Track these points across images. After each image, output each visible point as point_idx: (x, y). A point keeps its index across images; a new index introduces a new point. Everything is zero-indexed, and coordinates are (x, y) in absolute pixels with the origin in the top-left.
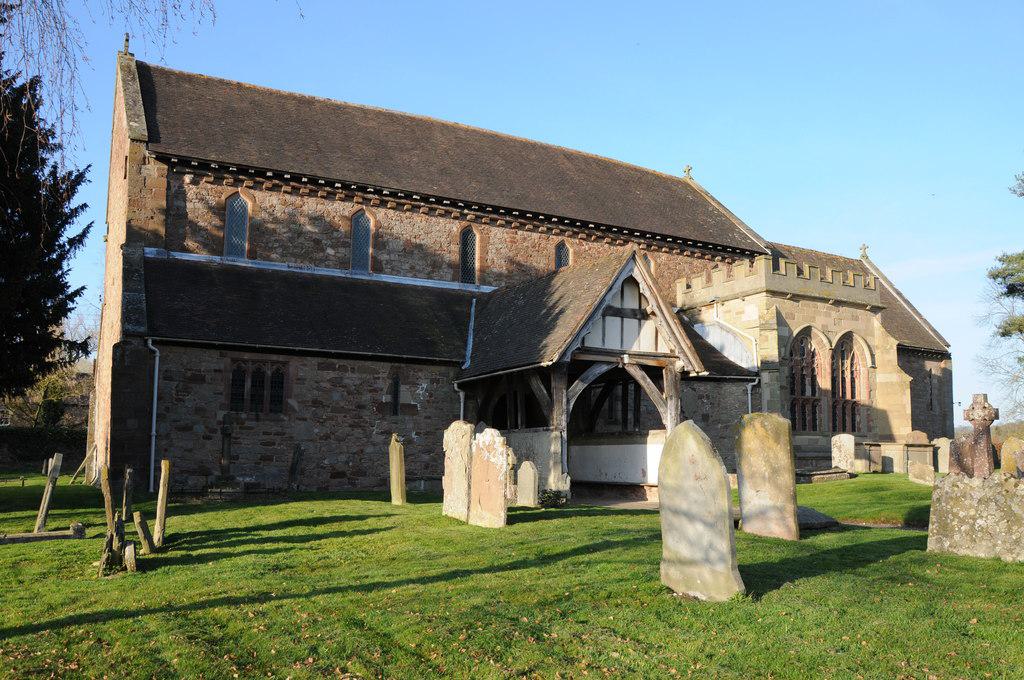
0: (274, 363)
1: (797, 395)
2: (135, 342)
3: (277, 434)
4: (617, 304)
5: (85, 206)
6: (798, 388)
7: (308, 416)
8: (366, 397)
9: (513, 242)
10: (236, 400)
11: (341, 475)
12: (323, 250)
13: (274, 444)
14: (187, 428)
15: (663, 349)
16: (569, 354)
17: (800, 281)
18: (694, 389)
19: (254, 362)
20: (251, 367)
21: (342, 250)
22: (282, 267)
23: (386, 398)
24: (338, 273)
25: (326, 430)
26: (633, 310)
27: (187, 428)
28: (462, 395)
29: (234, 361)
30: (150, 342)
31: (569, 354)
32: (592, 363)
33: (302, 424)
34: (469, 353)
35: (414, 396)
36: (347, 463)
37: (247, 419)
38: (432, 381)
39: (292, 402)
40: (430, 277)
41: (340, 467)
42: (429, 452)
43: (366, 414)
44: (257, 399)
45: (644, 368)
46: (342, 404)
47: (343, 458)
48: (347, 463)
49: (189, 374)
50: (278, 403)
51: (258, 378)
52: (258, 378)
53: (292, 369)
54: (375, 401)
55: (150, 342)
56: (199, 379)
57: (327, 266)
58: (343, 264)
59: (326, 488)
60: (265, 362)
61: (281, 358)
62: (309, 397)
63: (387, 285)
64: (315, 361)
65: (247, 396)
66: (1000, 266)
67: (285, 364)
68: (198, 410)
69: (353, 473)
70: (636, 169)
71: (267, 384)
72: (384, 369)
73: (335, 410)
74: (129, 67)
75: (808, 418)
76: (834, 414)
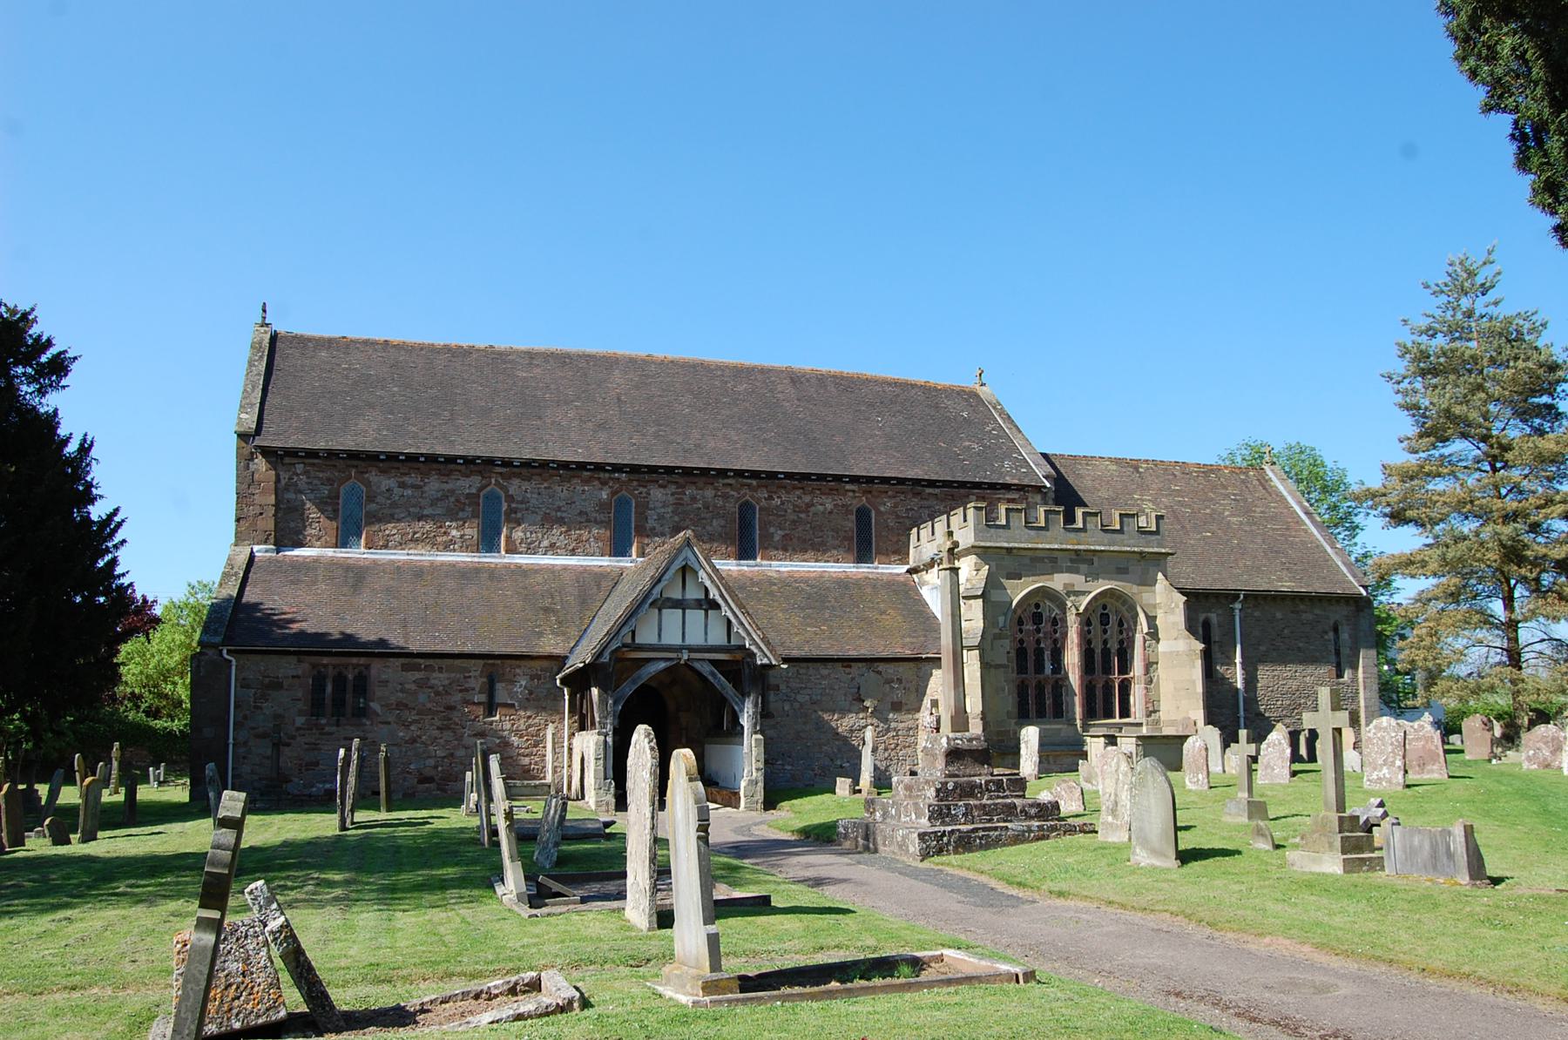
2: (210, 652)
5: (124, 541)
9: (678, 504)
11: (430, 780)
16: (607, 655)
18: (879, 673)
20: (331, 672)
26: (698, 601)
29: (314, 666)
31: (607, 655)
33: (385, 728)
35: (512, 695)
36: (436, 767)
37: (328, 724)
38: (532, 679)
39: (374, 705)
40: (573, 552)
41: (428, 772)
44: (339, 703)
45: (713, 662)
46: (429, 706)
47: (431, 762)
48: (436, 767)
51: (340, 680)
52: (340, 680)
53: (373, 672)
56: (277, 685)
58: (466, 548)
59: (413, 795)
61: (362, 660)
62: (393, 700)
63: (519, 567)
65: (328, 701)
69: (442, 779)
70: (896, 384)
71: (350, 688)
74: (260, 343)
75: (1048, 702)
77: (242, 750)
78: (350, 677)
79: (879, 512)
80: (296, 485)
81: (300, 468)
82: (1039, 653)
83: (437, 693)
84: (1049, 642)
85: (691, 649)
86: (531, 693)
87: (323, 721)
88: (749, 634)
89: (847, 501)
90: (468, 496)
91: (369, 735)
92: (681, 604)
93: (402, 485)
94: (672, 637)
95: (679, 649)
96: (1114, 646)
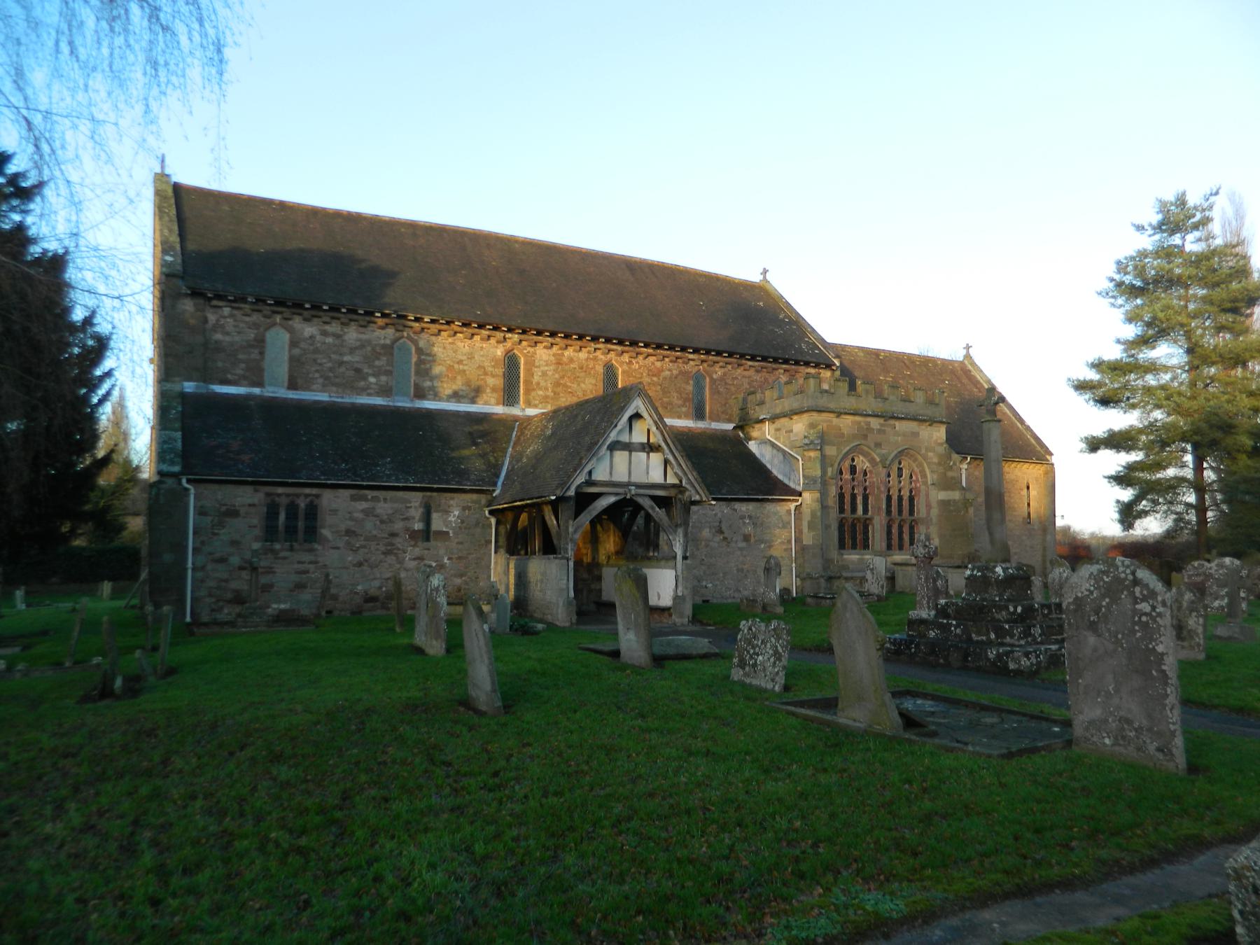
0: (307, 496)
1: (848, 514)
2: (170, 482)
3: (311, 563)
4: (625, 438)
6: (847, 506)
7: (341, 545)
8: (398, 526)
10: (270, 532)
12: (365, 379)
13: (308, 572)
14: (222, 560)
15: (671, 480)
17: (853, 399)
19: (288, 495)
20: (284, 501)
21: (384, 378)
22: (323, 397)
23: (418, 526)
24: (379, 401)
25: (360, 557)
26: (642, 444)
27: (222, 560)
28: (493, 521)
29: (268, 495)
30: (184, 481)
32: (598, 495)
34: (500, 483)
35: (447, 523)
36: (380, 588)
37: (282, 550)
38: (464, 509)
41: (373, 592)
42: (461, 576)
43: (398, 541)
45: (653, 498)
46: (374, 532)
47: (377, 583)
49: (224, 509)
50: (312, 533)
51: (292, 510)
52: (292, 510)
54: (407, 529)
55: (184, 481)
56: (233, 513)
57: (369, 395)
60: (298, 496)
61: (315, 491)
62: (343, 527)
64: (346, 493)
66: (1093, 376)
67: (317, 496)
68: (234, 543)
72: (416, 499)
73: (367, 539)
76: (889, 533)
77: (199, 574)
78: (302, 505)
79: (711, 378)
80: (223, 326)
81: (227, 311)
82: (854, 497)
83: (382, 522)
84: (861, 489)
85: (638, 486)
86: (462, 522)
87: (277, 546)
88: (685, 474)
89: (687, 367)
90: (384, 346)
91: (320, 559)
92: (629, 447)
93: (324, 333)
94: (621, 475)
95: (629, 484)
96: (905, 493)
